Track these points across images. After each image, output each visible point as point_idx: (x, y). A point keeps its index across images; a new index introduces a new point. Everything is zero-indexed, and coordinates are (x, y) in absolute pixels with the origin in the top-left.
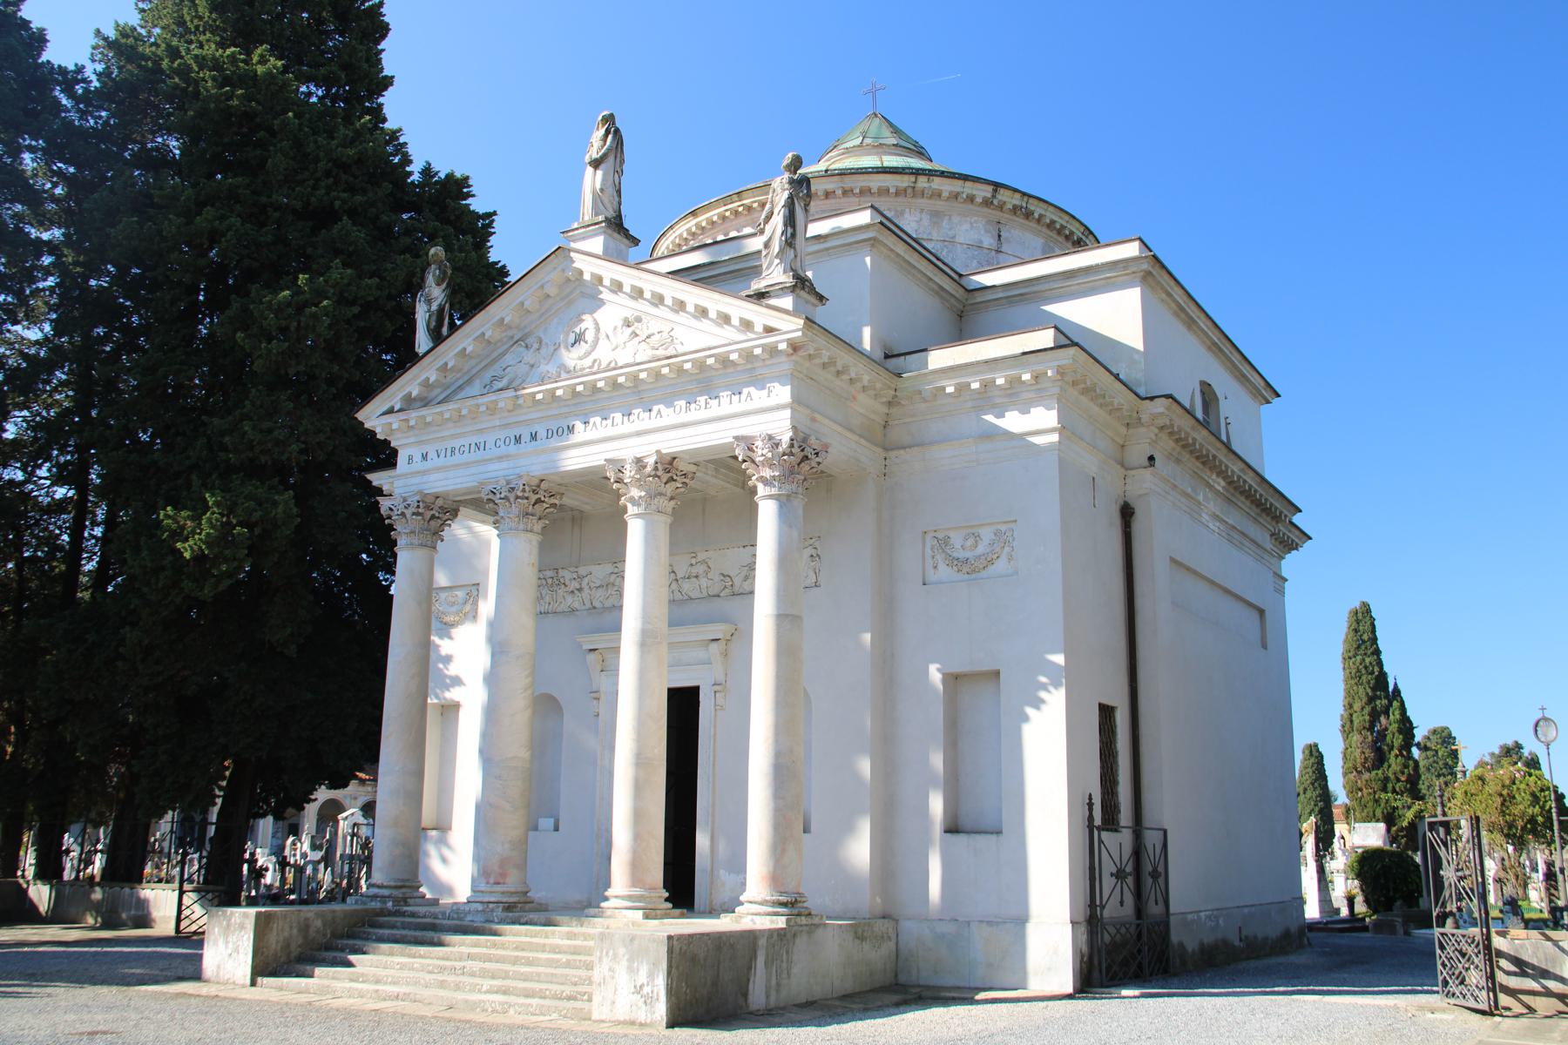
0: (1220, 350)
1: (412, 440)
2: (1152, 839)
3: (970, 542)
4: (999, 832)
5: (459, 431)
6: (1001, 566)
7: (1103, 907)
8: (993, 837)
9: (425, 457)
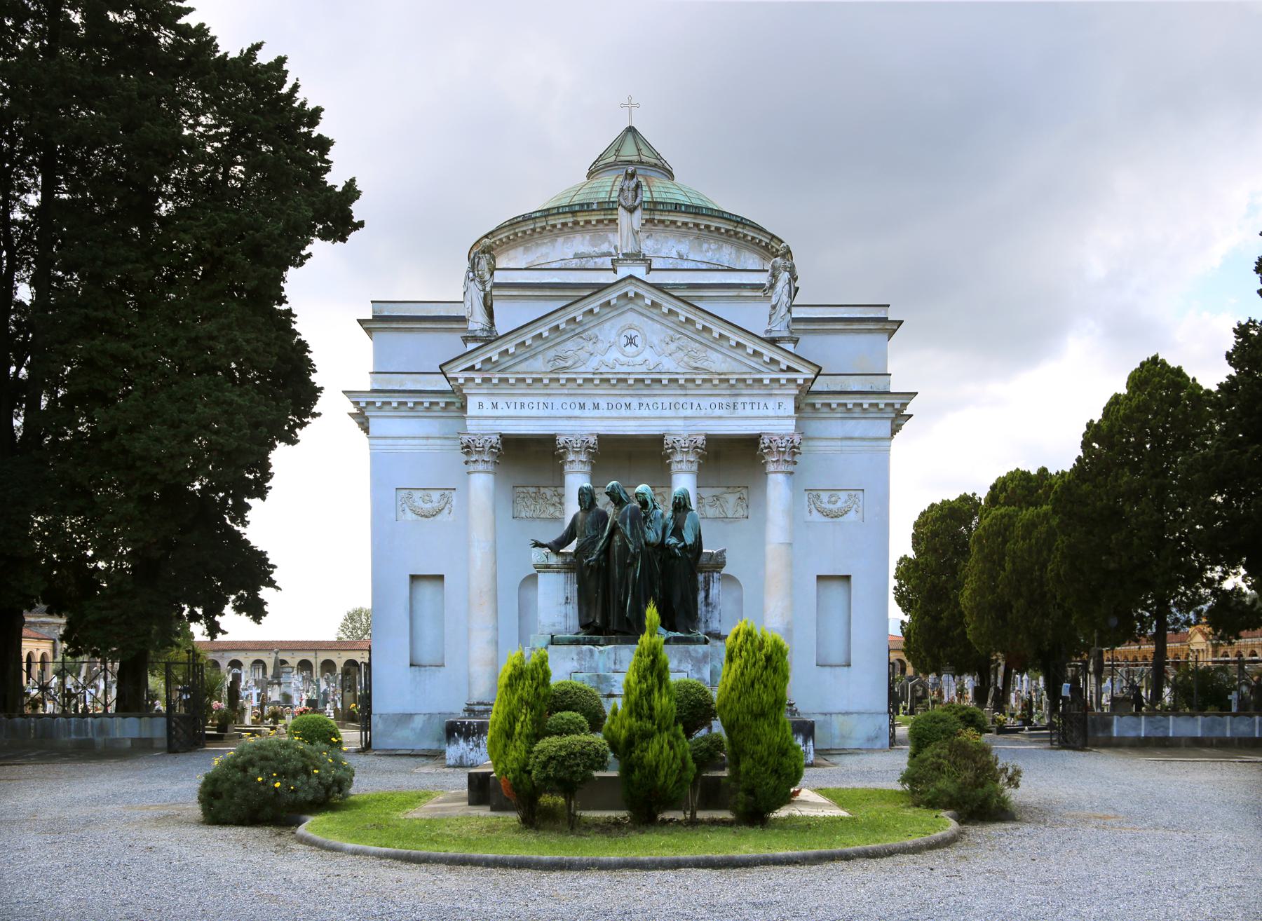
9: (495, 406)
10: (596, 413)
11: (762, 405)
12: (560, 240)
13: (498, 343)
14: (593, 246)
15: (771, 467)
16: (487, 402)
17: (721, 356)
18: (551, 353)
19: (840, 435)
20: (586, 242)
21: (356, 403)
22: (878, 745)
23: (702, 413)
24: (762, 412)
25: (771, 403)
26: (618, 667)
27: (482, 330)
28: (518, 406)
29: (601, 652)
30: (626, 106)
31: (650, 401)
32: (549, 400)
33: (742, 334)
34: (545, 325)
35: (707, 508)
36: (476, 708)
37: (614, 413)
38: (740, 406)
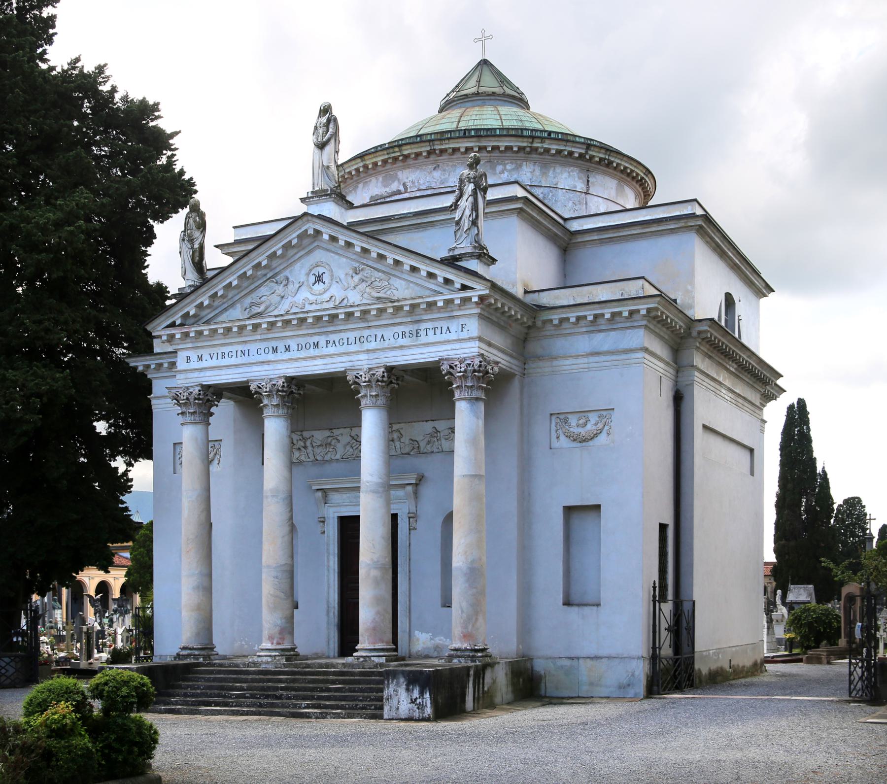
0: (739, 268)
2: (686, 607)
3: (581, 422)
4: (598, 605)
5: (228, 341)
6: (602, 439)
7: (660, 648)
8: (595, 608)
9: (200, 358)
10: (287, 356)
11: (444, 330)
12: (361, 186)
14: (385, 186)
15: (457, 395)
16: (193, 355)
17: (403, 283)
18: (248, 301)
19: (588, 350)
20: (380, 184)
22: (631, 692)
23: (386, 344)
24: (446, 336)
25: (454, 326)
28: (220, 356)
30: (479, 40)
31: (335, 337)
32: (245, 348)
33: (413, 256)
34: (232, 274)
35: (443, 441)
37: (303, 354)
38: (423, 333)
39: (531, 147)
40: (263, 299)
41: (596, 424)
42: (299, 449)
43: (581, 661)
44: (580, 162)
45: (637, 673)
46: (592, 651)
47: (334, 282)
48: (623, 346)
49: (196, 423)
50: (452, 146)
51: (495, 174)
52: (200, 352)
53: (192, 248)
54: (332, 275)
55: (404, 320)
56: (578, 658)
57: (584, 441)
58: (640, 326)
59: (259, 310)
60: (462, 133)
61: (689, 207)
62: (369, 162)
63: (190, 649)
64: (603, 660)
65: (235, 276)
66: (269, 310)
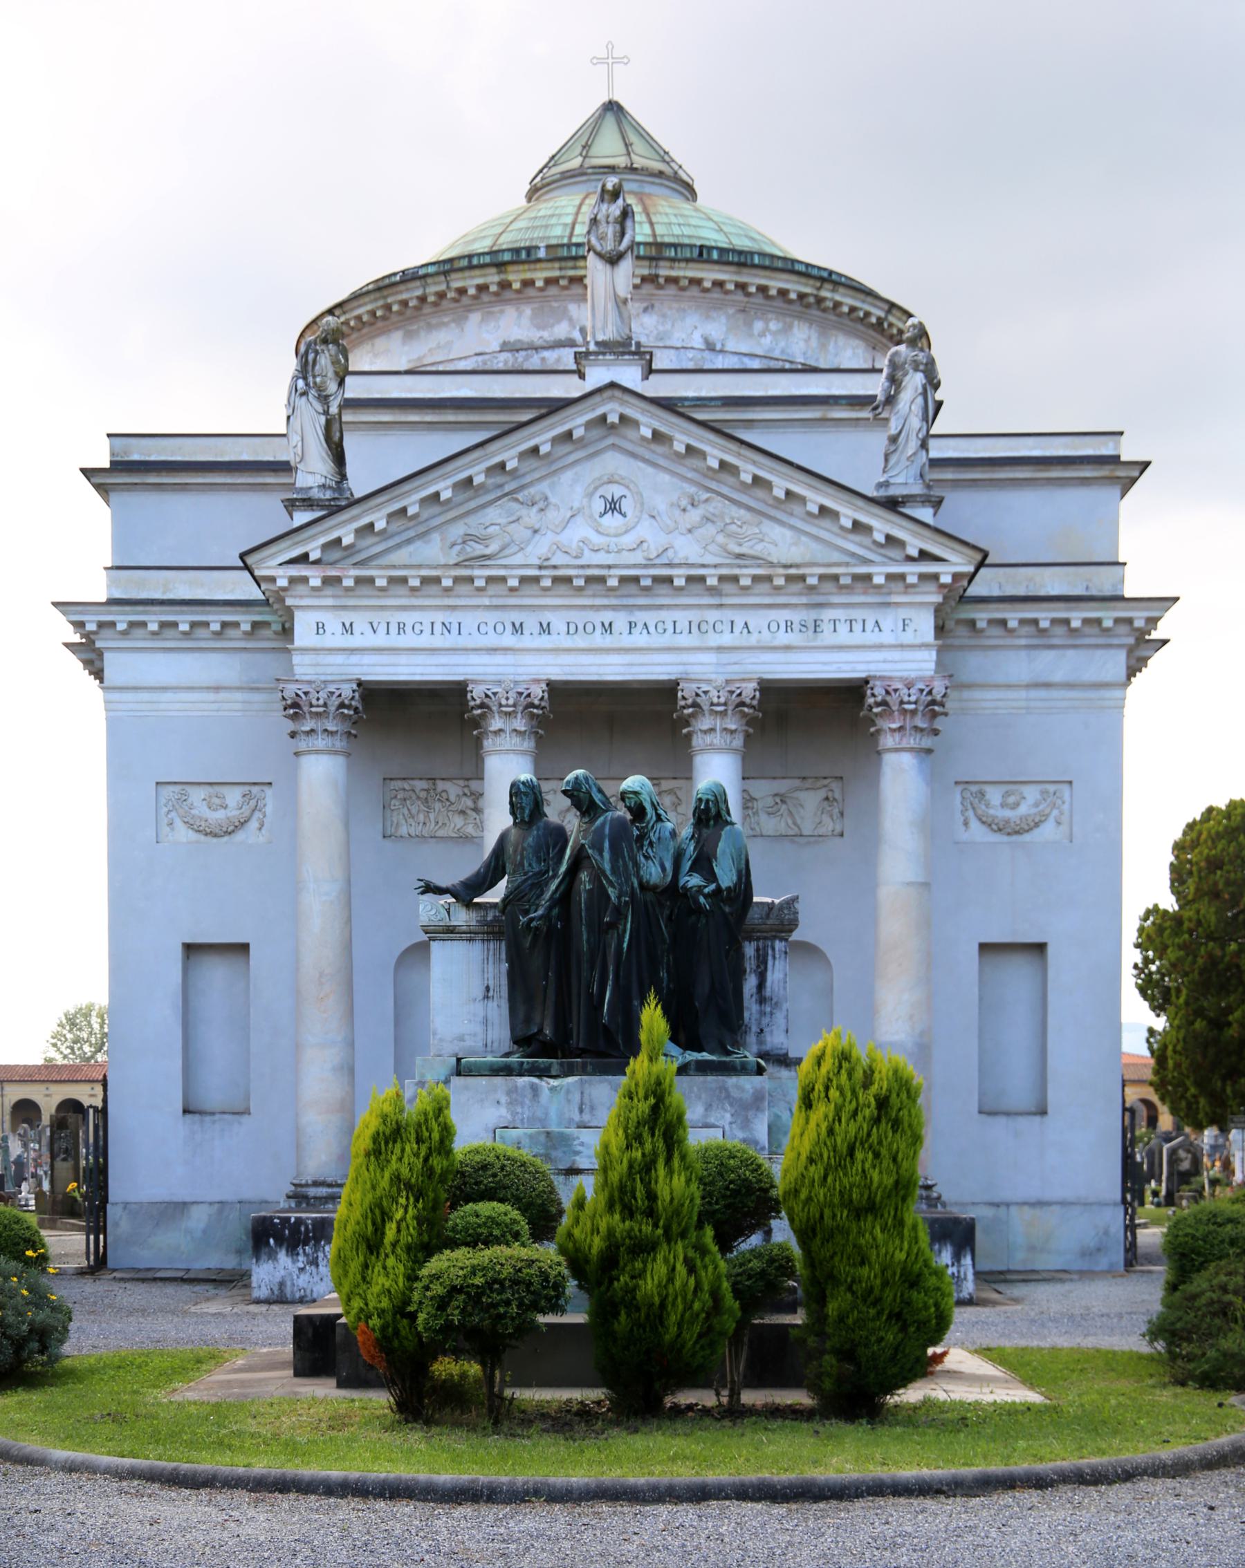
1: (330, 602)
3: (1011, 800)
6: (1048, 831)
9: (348, 629)
10: (545, 641)
12: (475, 317)
13: (355, 511)
14: (540, 327)
15: (888, 741)
16: (333, 622)
17: (788, 533)
19: (1025, 678)
21: (79, 625)
22: (1103, 1263)
23: (753, 640)
24: (872, 637)
25: (889, 620)
26: (586, 1117)
27: (323, 487)
29: (553, 1089)
31: (651, 617)
32: (453, 618)
34: (444, 477)
35: (763, 817)
36: (312, 1192)
37: (580, 641)
38: (826, 627)
39: (816, 296)
40: (491, 530)
41: (1036, 805)
42: (463, 812)
43: (1013, 1209)
44: (871, 332)
45: (1113, 1230)
46: (1033, 1192)
47: (645, 516)
48: (1089, 675)
49: (336, 753)
50: (690, 274)
51: (751, 335)
52: (348, 617)
53: (326, 413)
54: (642, 504)
55: (794, 600)
56: (1008, 1205)
57: (1017, 833)
58: (1120, 646)
59: (488, 551)
60: (696, 253)
61: (1111, 445)
62: (515, 277)
63: (330, 1185)
64: (1054, 1208)
65: (450, 482)
66: (507, 552)
